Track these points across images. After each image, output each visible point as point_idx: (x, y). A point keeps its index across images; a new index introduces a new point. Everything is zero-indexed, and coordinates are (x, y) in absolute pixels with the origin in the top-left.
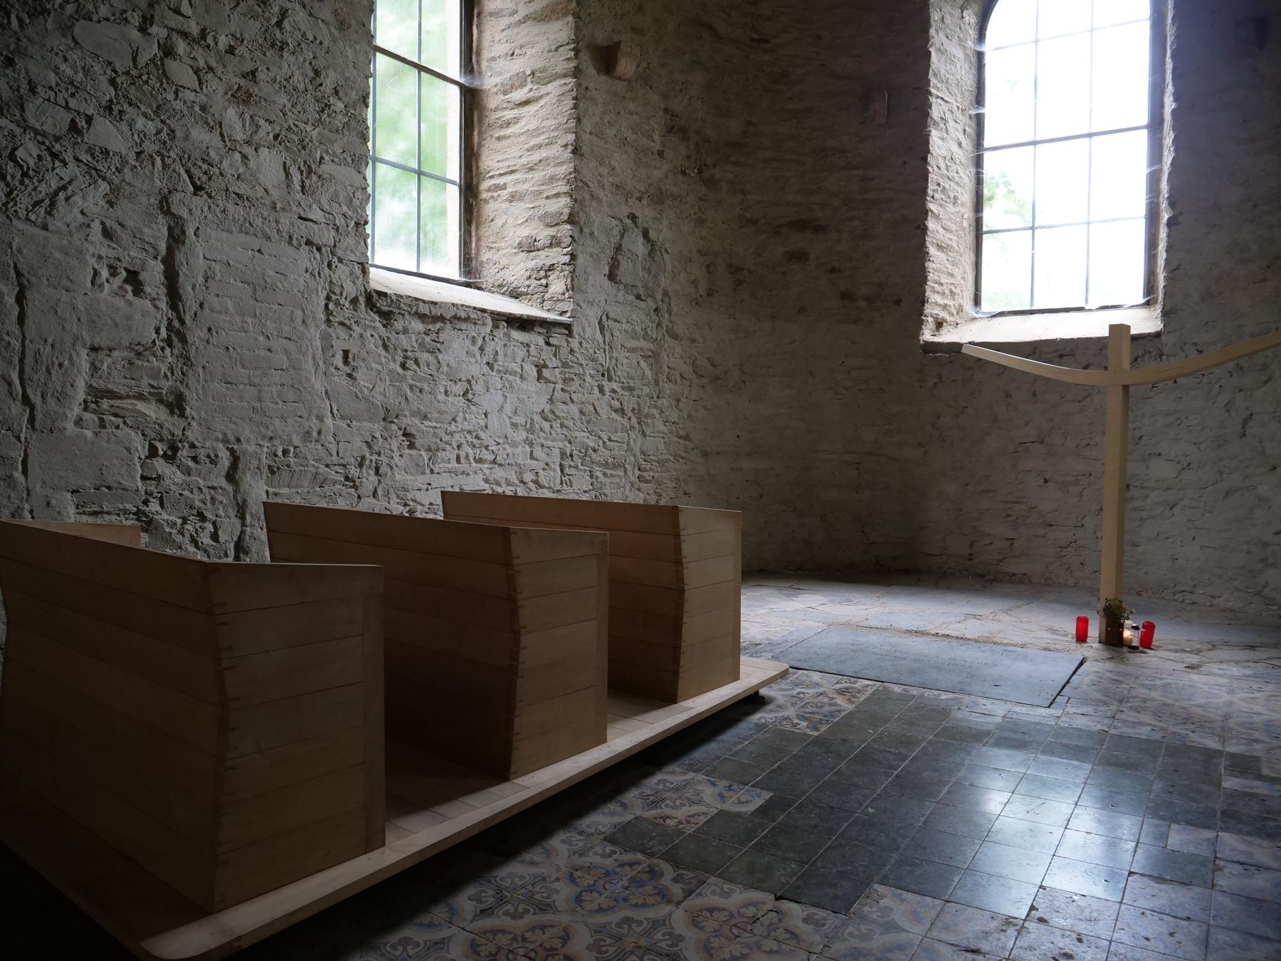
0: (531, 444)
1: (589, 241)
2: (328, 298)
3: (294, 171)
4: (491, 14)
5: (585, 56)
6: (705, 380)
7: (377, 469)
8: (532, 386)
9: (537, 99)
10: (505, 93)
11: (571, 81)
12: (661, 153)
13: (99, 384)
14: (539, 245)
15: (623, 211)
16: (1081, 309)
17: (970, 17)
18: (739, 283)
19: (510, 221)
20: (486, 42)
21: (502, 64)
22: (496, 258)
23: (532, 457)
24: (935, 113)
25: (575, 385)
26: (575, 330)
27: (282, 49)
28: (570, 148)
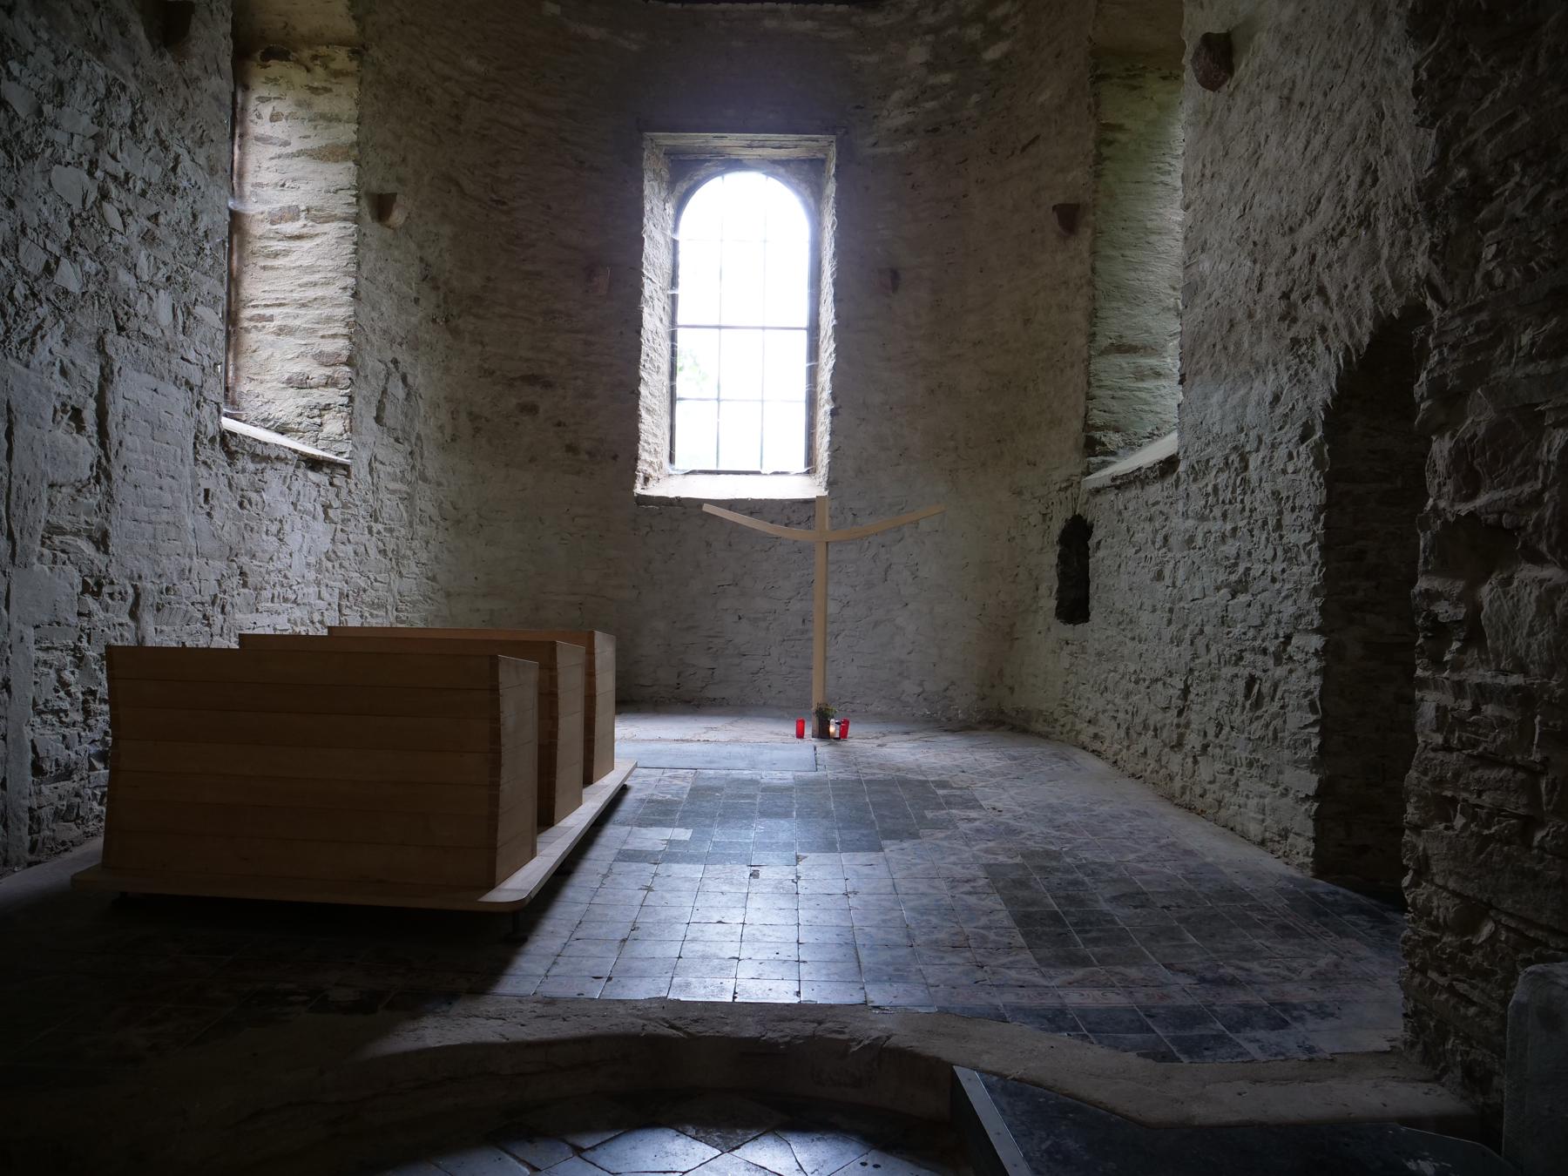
0: (319, 584)
1: (363, 385)
2: (196, 437)
3: (179, 313)
4: (257, 139)
5: (363, 203)
6: (448, 523)
7: (223, 608)
8: (320, 526)
9: (311, 237)
10: (273, 223)
11: (352, 227)
12: (417, 301)
13: (54, 520)
14: (312, 382)
15: (388, 356)
16: (758, 473)
17: (670, 210)
18: (477, 430)
19: (277, 355)
20: (251, 165)
21: (268, 193)
22: (259, 390)
23: (320, 598)
24: (647, 292)
25: (351, 526)
26: (353, 471)
27: (174, 193)
28: (349, 292)
